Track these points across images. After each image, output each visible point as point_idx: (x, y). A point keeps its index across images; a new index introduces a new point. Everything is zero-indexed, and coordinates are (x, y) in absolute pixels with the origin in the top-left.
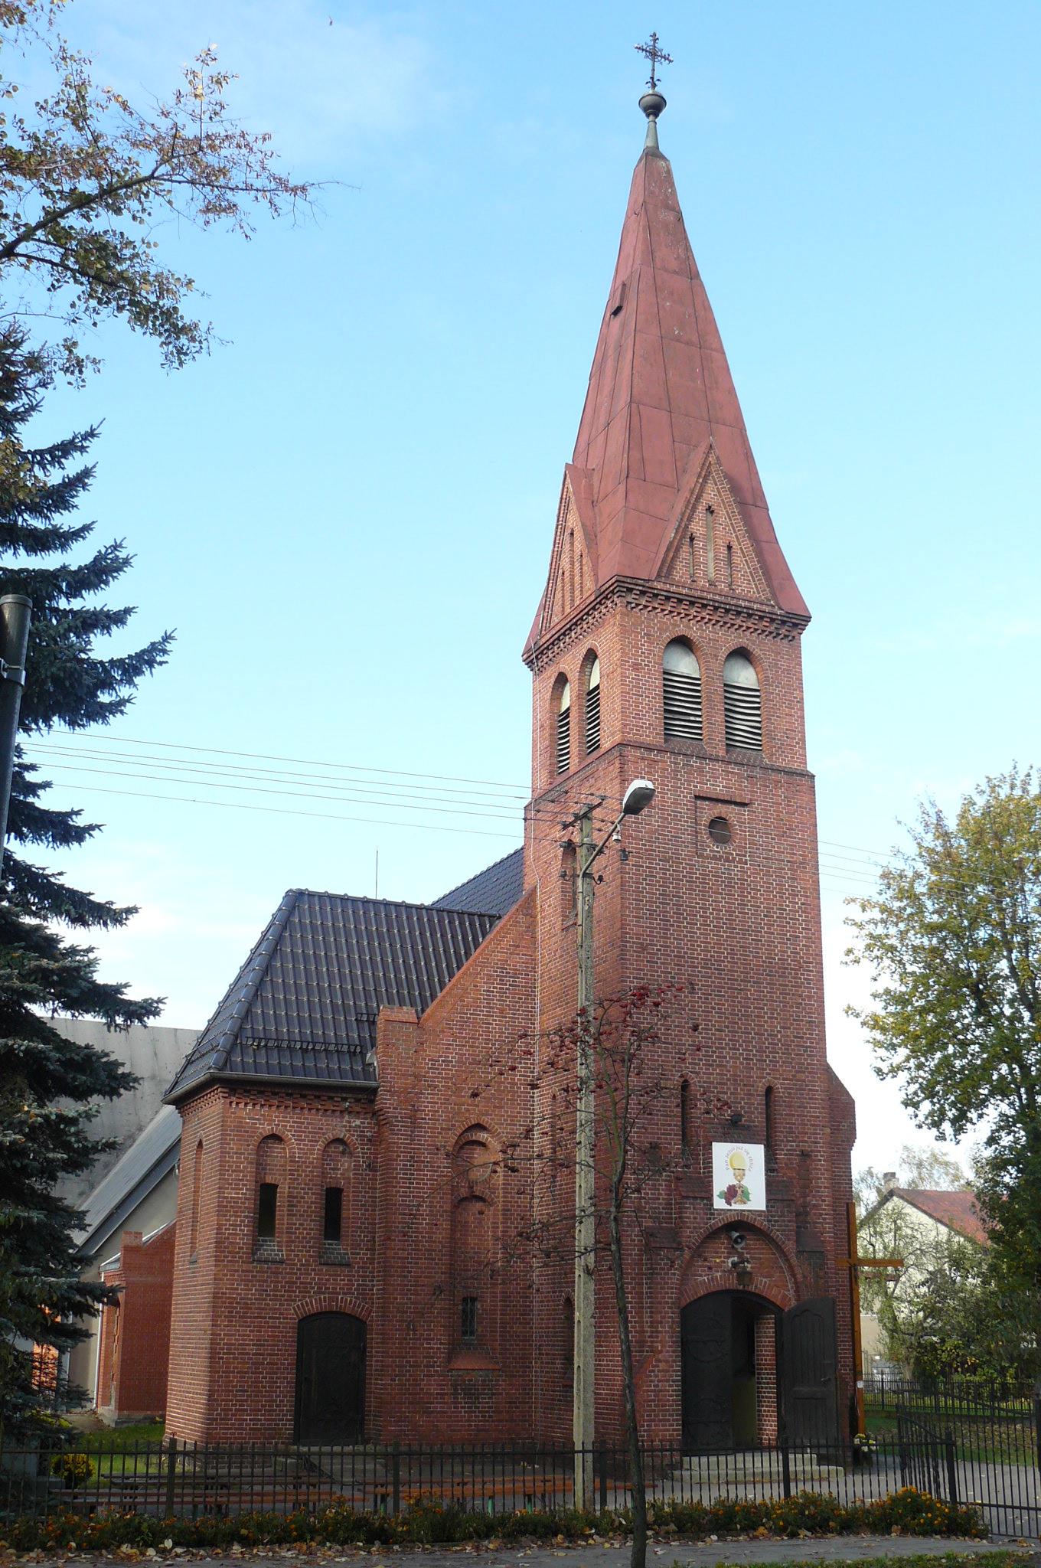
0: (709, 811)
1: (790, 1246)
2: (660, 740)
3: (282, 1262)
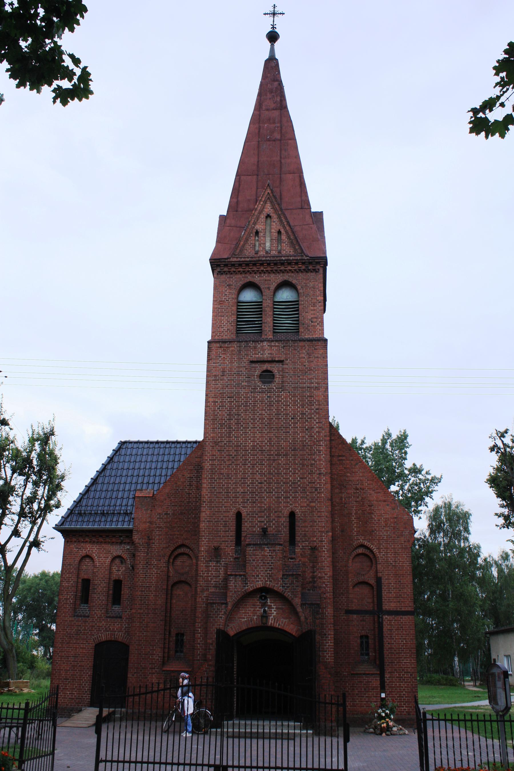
0: (259, 369)
1: (297, 601)
2: (234, 336)
3: (88, 616)
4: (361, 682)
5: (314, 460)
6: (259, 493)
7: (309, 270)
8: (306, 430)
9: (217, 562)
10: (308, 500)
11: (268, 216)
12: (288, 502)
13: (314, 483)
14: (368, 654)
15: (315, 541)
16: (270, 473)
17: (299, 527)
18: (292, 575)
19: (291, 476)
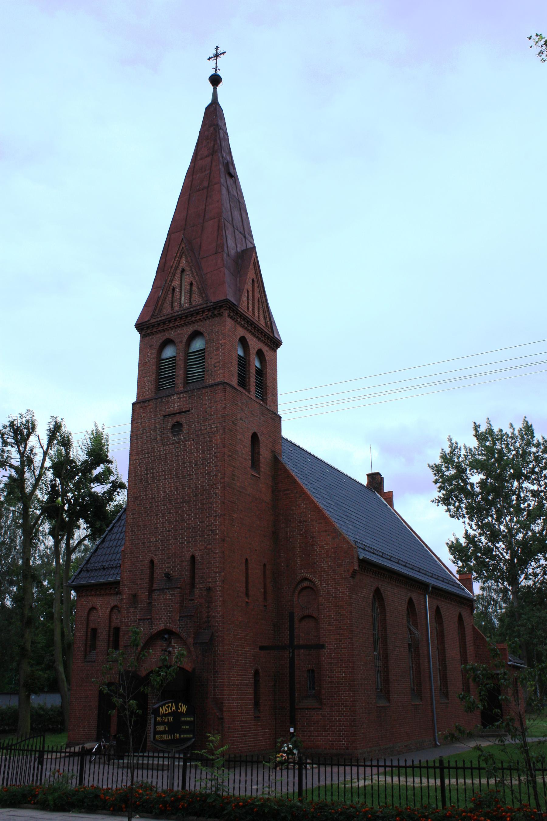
3: (94, 662)
4: (304, 716)
5: (211, 503)
6: (167, 540)
7: (215, 315)
8: (206, 474)
9: (135, 607)
10: (205, 543)
11: (183, 271)
12: (190, 547)
13: (211, 526)
14: (314, 689)
15: (210, 582)
16: (176, 521)
17: (198, 569)
18: (187, 616)
19: (192, 521)
